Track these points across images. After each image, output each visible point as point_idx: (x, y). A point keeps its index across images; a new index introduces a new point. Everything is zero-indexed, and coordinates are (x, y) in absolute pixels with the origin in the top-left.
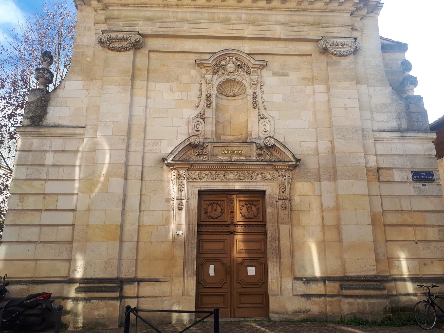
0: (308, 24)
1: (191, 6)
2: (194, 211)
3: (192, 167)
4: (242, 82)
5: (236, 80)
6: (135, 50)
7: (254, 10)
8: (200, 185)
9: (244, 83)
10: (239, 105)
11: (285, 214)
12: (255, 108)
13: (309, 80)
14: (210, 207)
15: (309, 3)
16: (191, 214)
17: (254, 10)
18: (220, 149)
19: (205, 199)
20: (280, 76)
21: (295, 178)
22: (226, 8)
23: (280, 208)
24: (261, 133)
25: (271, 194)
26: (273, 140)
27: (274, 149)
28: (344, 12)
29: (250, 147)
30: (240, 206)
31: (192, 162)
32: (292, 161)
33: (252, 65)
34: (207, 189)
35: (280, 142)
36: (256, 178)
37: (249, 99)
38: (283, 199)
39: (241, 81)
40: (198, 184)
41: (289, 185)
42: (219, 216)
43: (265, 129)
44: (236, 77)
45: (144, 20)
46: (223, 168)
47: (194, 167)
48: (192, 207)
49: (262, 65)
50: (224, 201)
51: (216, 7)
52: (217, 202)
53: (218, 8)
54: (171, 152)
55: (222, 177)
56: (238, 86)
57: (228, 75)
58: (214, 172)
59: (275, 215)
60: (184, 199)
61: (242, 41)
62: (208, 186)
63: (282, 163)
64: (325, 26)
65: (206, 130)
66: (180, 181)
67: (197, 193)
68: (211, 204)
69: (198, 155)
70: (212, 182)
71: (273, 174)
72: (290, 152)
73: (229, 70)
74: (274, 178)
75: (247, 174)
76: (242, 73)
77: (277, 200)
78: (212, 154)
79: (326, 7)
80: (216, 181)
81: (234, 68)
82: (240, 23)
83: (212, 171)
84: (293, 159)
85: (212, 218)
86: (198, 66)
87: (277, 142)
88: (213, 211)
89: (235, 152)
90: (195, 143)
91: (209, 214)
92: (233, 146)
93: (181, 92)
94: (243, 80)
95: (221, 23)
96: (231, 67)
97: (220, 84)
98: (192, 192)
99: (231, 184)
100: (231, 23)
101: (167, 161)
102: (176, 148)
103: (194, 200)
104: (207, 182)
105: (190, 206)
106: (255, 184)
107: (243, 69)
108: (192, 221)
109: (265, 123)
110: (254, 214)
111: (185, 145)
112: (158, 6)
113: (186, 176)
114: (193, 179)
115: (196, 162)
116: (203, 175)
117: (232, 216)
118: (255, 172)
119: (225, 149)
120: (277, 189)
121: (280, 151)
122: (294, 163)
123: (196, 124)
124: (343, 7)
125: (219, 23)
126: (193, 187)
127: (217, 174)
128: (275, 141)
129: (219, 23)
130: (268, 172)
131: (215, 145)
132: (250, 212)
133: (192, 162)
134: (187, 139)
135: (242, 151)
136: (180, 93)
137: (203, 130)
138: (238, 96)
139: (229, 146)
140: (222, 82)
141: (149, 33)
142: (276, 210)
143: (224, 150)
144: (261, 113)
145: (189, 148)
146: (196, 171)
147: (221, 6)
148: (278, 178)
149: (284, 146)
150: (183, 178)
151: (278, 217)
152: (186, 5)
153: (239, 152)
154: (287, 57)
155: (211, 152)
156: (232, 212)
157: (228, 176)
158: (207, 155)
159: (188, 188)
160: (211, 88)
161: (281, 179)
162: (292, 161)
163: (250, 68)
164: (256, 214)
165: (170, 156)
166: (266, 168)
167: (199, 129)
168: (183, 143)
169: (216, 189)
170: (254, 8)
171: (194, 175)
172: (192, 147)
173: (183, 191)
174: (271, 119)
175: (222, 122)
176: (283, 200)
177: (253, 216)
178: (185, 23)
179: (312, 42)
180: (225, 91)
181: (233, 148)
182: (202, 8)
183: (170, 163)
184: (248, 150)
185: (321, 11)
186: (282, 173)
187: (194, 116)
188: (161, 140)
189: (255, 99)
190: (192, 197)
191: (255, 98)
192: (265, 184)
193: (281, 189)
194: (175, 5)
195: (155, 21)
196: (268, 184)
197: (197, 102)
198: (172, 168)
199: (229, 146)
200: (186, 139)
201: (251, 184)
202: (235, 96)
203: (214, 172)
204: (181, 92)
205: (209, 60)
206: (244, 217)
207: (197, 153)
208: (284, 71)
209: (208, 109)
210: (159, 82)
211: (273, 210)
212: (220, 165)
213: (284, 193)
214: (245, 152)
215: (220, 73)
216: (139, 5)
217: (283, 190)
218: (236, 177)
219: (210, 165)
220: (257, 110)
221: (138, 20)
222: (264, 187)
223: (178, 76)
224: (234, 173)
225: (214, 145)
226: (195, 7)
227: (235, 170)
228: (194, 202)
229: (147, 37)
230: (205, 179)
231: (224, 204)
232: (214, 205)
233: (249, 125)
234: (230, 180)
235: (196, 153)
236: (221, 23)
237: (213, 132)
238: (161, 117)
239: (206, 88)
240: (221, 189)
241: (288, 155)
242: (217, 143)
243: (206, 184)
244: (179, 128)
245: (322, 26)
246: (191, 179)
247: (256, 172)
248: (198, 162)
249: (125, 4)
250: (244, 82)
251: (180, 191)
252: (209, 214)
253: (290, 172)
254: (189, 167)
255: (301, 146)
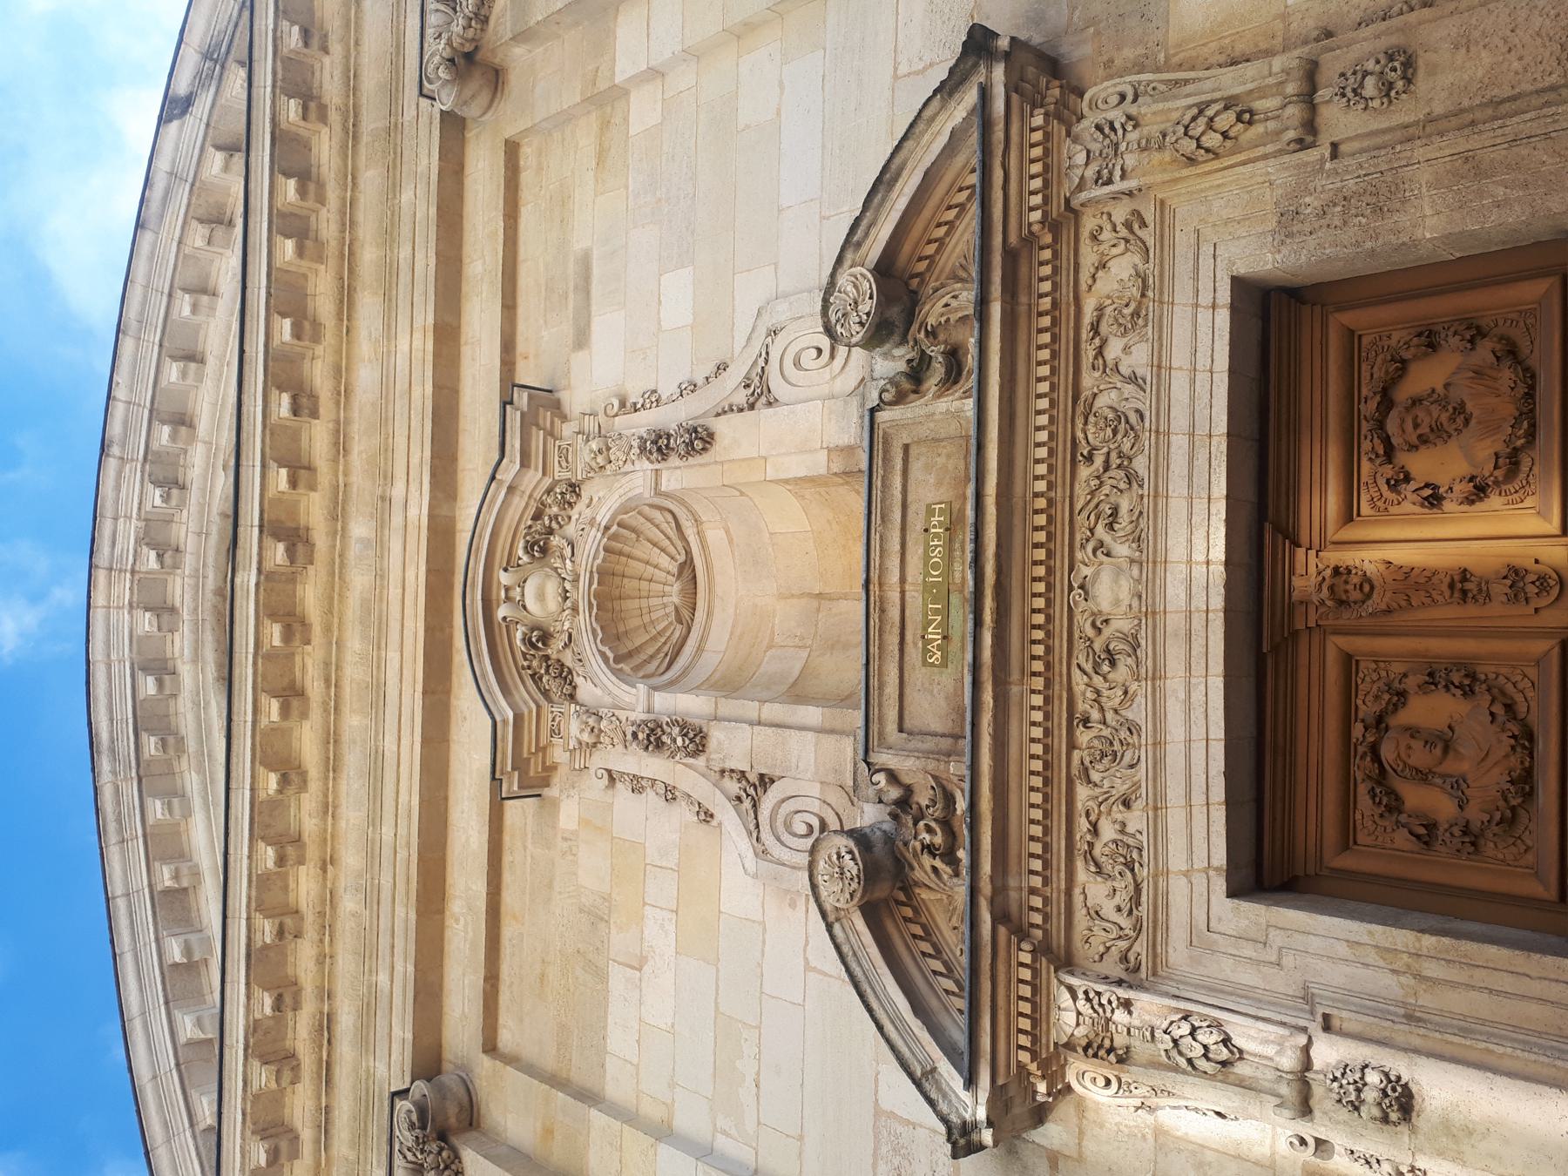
0: (392, 187)
1: (326, 796)
2: (1432, 969)
3: (1037, 919)
4: (607, 528)
5: (599, 561)
6: (479, 1126)
7: (346, 475)
8: (1187, 874)
9: (608, 517)
10: (731, 541)
11: (1464, 43)
12: (711, 435)
13: (605, 125)
14: (1415, 796)
15: (310, 203)
16: (1457, 1002)
17: (346, 475)
18: (917, 675)
19: (1331, 832)
20: (588, 305)
21: (1141, 51)
22: (336, 620)
23: (1405, 112)
24: (838, 382)
25: (1272, 223)
26: (843, 280)
27: (920, 259)
28: (357, 18)
29: (906, 448)
30: (1407, 507)
31: (986, 917)
32: (985, 93)
33: (531, 472)
34: (1219, 815)
35: (857, 221)
36: (1133, 379)
37: (678, 476)
38: (1308, 98)
39: (599, 535)
40: (1178, 891)
41: (1186, 82)
42: (1498, 709)
43: (820, 351)
44: (583, 567)
45: (367, 1051)
46: (1038, 666)
47: (1037, 902)
48: (1387, 984)
49: (537, 415)
50: (1349, 662)
51: (334, 667)
52: (1357, 730)
53: (338, 659)
54: (911, 1075)
55: (1121, 673)
56: (637, 553)
57: (575, 609)
58: (1083, 737)
59: (1476, 141)
60: (1306, 1049)
61: (458, 535)
62: (1198, 798)
63: (998, 175)
64: (397, 99)
65: (812, 768)
66: (1141, 1049)
67: (1253, 913)
68: (1381, 775)
69: (950, 857)
70: (1159, 764)
71: (1106, 235)
72: (921, 126)
73: (553, 603)
74: (1136, 226)
75: (1099, 461)
76: (570, 530)
77: (1322, 161)
78: (946, 743)
79: (334, 117)
80: (1147, 728)
81: (548, 576)
82: (382, 547)
83: (1076, 754)
84: (970, 97)
85: (1525, 781)
86: (548, 785)
87: (859, 245)
88: (1451, 766)
89: (935, 566)
90: (855, 872)
91: (1475, 815)
92: (894, 577)
93: (645, 904)
94: (598, 519)
95: (379, 648)
96: (541, 596)
97: (617, 660)
98: (1248, 951)
99: (1175, 594)
100: (381, 592)
101: (975, 1125)
102: (889, 1027)
103: (1315, 944)
104: (1157, 808)
105: (1372, 997)
106: (1179, 385)
107: (554, 525)
108: (1534, 1009)
109: (789, 362)
110: (1478, 373)
111: (874, 950)
112: (327, 959)
113: (1100, 988)
114: (1138, 928)
115: (986, 887)
116: (1108, 832)
117: (1500, 589)
118: (1086, 394)
119: (915, 644)
120: (1217, 179)
121: (927, 213)
122: (999, 72)
123: (786, 837)
124: (334, 25)
125: (379, 658)
126: (1202, 937)
127: (1095, 715)
128: (849, 256)
129: (379, 658)
130: (1083, 287)
131: (892, 715)
132: (1460, 409)
133: (986, 917)
134: (829, 928)
135: (930, 512)
136: (648, 910)
137: (815, 790)
138: (688, 553)
139: (894, 613)
140: (606, 649)
141: (409, 1036)
142: (1419, 152)
143: (925, 651)
144: (741, 397)
145: (906, 919)
146: (1077, 891)
147: (331, 643)
148: (1131, 184)
149: (884, 181)
150: (1120, 1016)
151: (1500, 107)
152: (325, 821)
153: (937, 535)
154: (525, 280)
155: (927, 754)
156: (1462, 584)
157: (1116, 624)
158: (949, 787)
159: (1212, 990)
160: (622, 715)
161: (1130, 160)
162: (985, 93)
163: (547, 482)
164: (1484, 352)
165: (939, 1089)
166: (1046, 303)
167: (816, 823)
168: (854, 965)
169: (1218, 731)
170: (337, 476)
171: (1108, 910)
172: (902, 897)
173: (1226, 1041)
174: (767, 322)
175: (805, 655)
176: (1323, 94)
177: (1506, 376)
178: (378, 837)
179: (463, 153)
180: (665, 629)
181: (909, 579)
182: (335, 742)
183: (992, 1103)
184: (928, 468)
185: (351, 133)
186: (1080, 158)
187: (744, 845)
188: (878, 1112)
189: (669, 436)
190: (1288, 961)
191: (659, 446)
192: (1182, 293)
193: (1211, 140)
194: (325, 879)
195: (370, 993)
196: (1183, 267)
197: (683, 813)
198: (1042, 1087)
199: (894, 613)
200: (833, 937)
201: (1179, 419)
202: (687, 570)
203: (1083, 737)
204: (645, 904)
205: (498, 719)
206: (1511, 465)
207: (938, 863)
208: (571, 285)
209: (712, 744)
210: (605, 1028)
211: (1425, 175)
212: (1015, 690)
213: (1259, 105)
214: (939, 484)
215: (568, 659)
216: (325, 1058)
217: (1226, 120)
218: (1123, 550)
219: (1013, 769)
220: (721, 427)
221: (367, 1079)
222: (1205, 298)
223: (581, 911)
224: (1086, 571)
225: (891, 726)
226: (331, 775)
227: (1061, 563)
228: (1342, 950)
229: (440, 1046)
230: (1136, 820)
231: (1378, 659)
232: (1387, 752)
233: (797, 467)
234: (1148, 610)
235: (935, 869)
236: (379, 648)
237: (827, 726)
238: (758, 1074)
239: (620, 747)
240: (1217, 684)
241: (943, 140)
242: (874, 701)
243: (1175, 818)
244: (813, 964)
245: (397, 115)
246: (1137, 948)
247: (1089, 380)
248: (986, 867)
249: (320, 1126)
250: (603, 517)
251: (1224, 1064)
252: (1475, 815)
253: (1087, 96)
254: (1026, 946)
255: (925, 69)
